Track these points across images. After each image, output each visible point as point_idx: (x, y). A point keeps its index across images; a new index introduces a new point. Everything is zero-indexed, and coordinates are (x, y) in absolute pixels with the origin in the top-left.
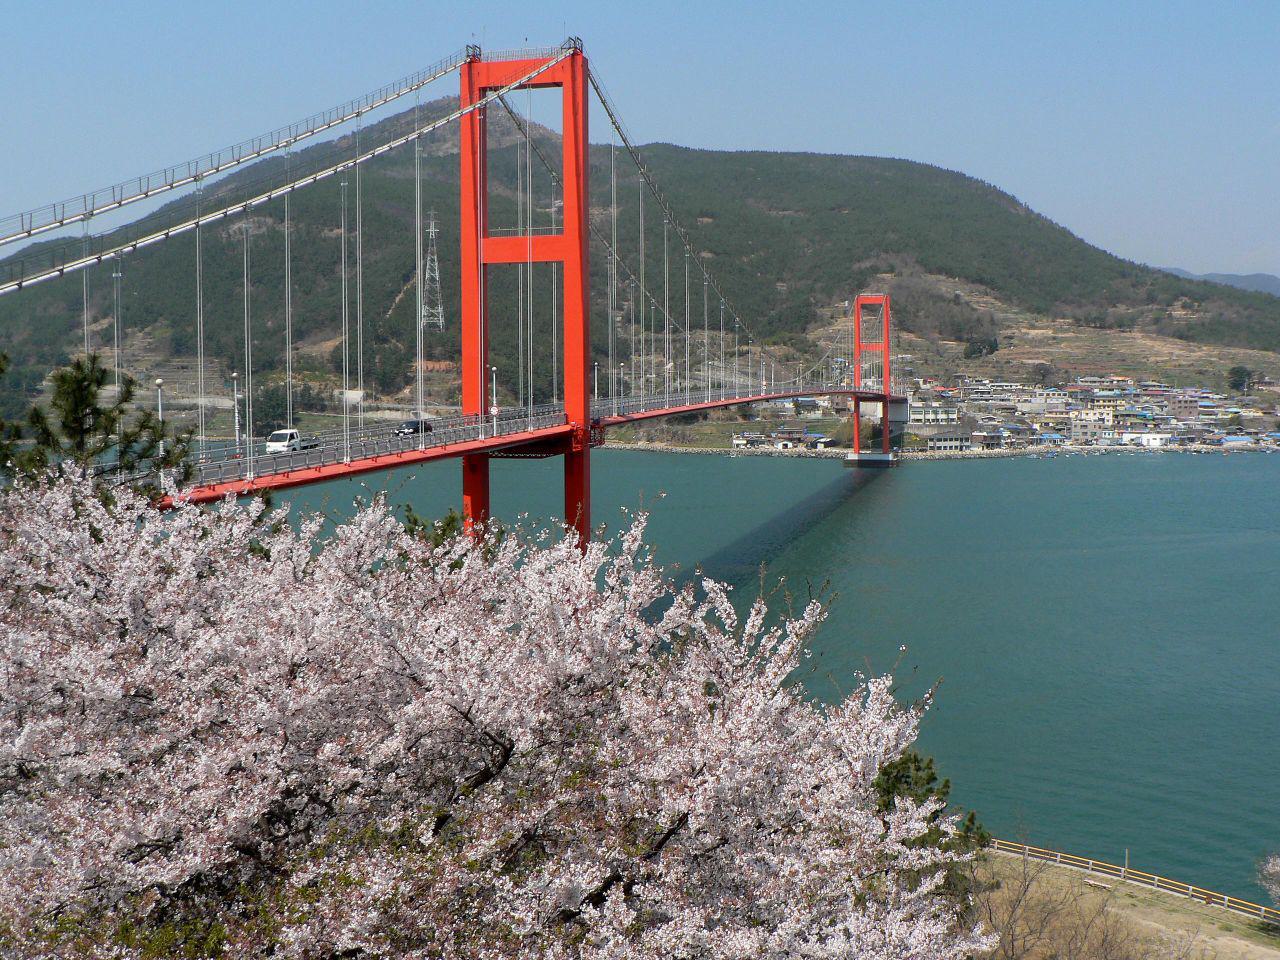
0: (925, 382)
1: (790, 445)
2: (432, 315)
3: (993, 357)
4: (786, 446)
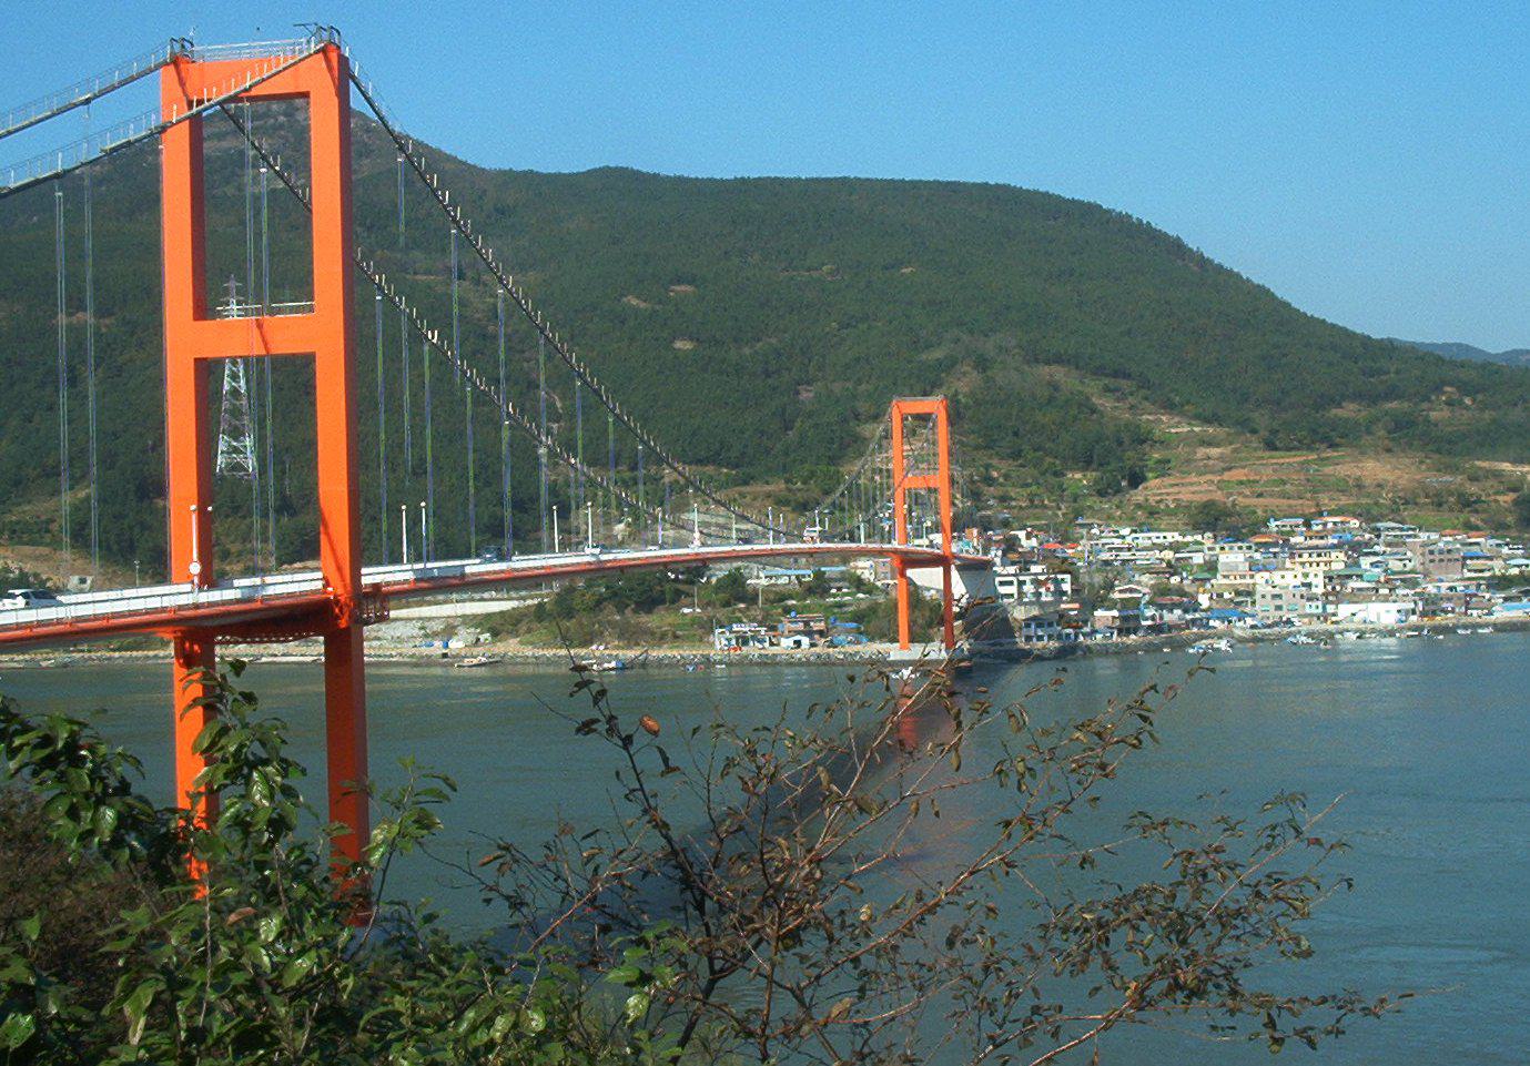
0: (1028, 537)
1: (805, 641)
2: (236, 450)
3: (1138, 495)
4: (798, 643)
